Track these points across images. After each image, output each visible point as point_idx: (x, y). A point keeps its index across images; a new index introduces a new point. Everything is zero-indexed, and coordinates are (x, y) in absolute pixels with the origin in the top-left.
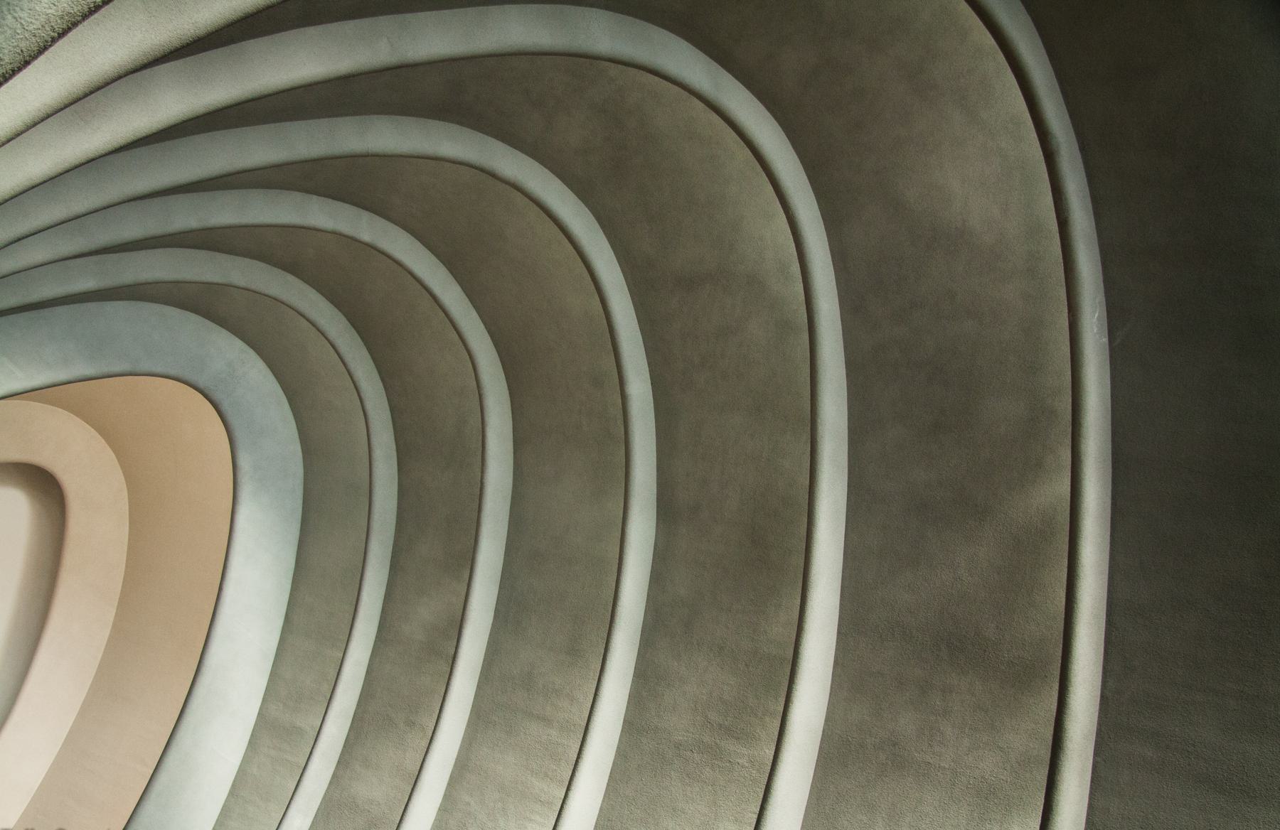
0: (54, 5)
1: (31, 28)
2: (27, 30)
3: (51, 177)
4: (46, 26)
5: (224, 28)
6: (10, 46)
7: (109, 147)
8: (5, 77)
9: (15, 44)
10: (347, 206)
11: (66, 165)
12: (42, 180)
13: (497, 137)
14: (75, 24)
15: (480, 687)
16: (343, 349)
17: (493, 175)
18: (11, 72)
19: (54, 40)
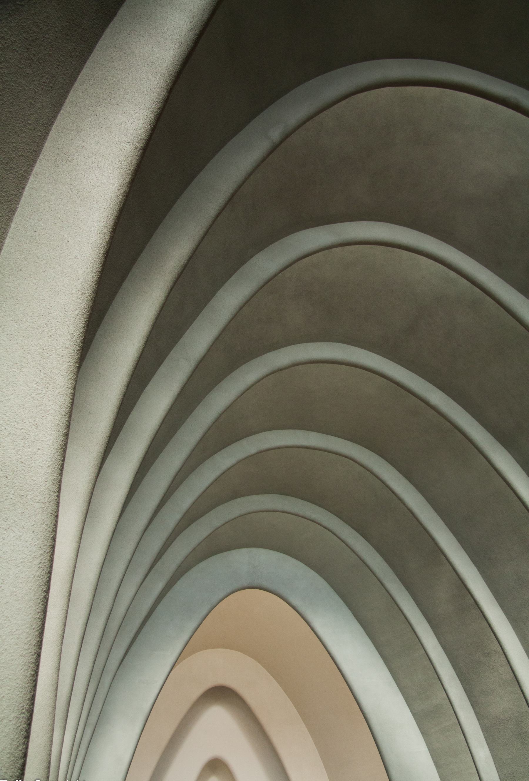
0: (46, 482)
1: (46, 500)
2: (46, 503)
3: (105, 554)
4: (51, 493)
5: (115, 422)
6: (45, 516)
7: (116, 519)
8: (54, 531)
9: (46, 513)
10: (233, 445)
11: (107, 543)
12: (103, 559)
13: (269, 351)
14: (60, 481)
15: (502, 607)
16: (290, 509)
17: (281, 370)
18: (55, 526)
19: (58, 496)
